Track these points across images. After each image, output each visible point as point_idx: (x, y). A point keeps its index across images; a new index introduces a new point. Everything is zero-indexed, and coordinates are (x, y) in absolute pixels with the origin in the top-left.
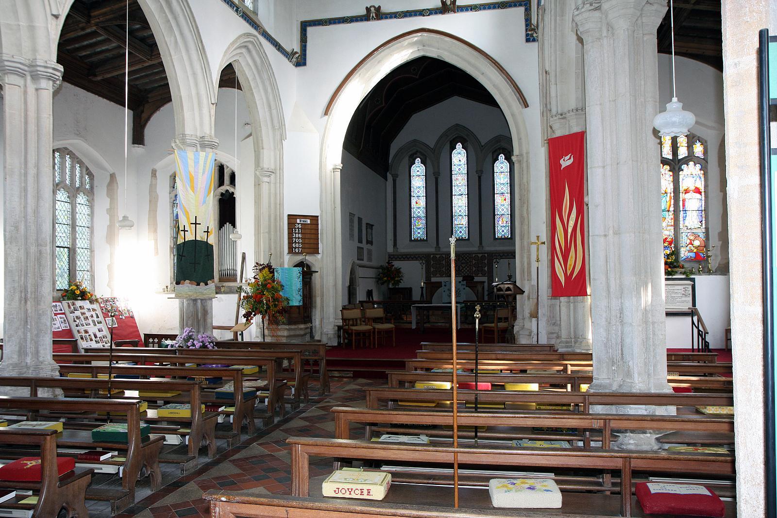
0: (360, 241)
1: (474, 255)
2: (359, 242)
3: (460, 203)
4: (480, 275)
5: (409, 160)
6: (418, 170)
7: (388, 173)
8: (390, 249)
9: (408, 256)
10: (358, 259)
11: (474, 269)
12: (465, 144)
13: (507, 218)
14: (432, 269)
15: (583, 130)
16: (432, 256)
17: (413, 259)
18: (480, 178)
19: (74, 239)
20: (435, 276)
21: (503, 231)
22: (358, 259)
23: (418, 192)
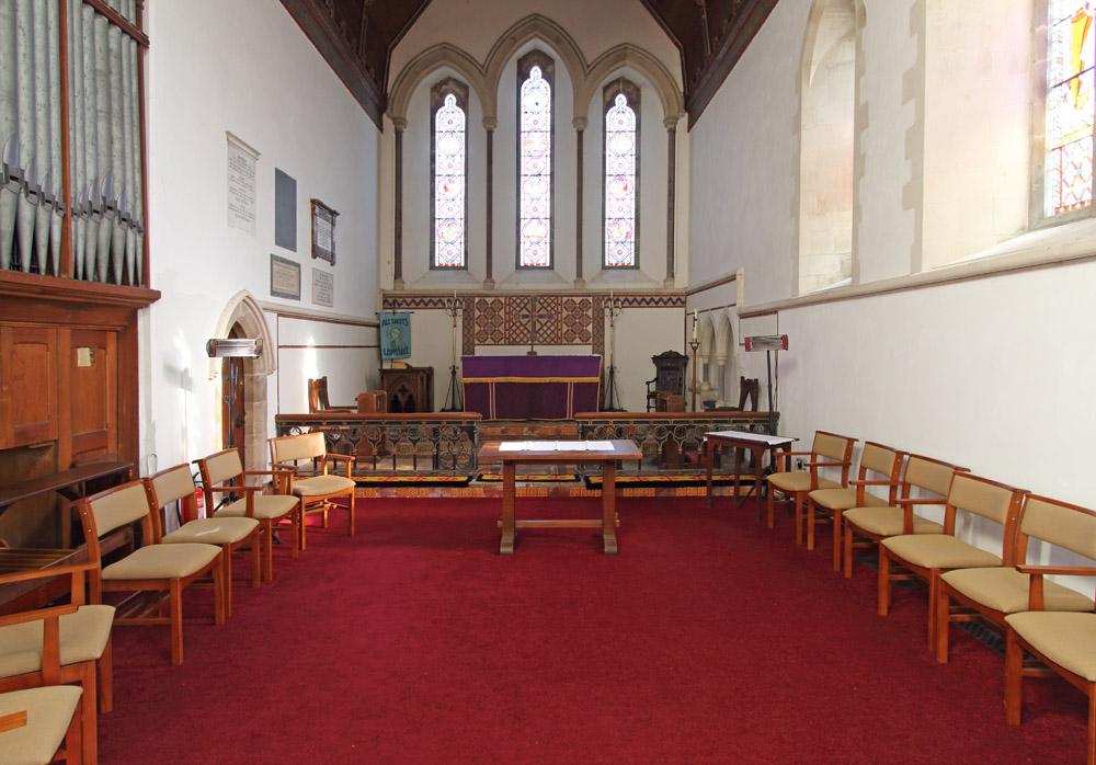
0: (286, 236)
1: (565, 299)
2: (278, 242)
3: (535, 195)
4: (577, 341)
5: (432, 97)
6: (451, 117)
7: (385, 116)
8: (388, 284)
9: (426, 300)
10: (273, 293)
11: (565, 328)
12: (549, 69)
13: (628, 227)
14: (477, 329)
15: (361, 392)
16: (477, 300)
17: (435, 306)
18: (490, 133)
19: (379, 339)
20: (483, 343)
21: (620, 253)
22: (273, 293)
23: (450, 166)
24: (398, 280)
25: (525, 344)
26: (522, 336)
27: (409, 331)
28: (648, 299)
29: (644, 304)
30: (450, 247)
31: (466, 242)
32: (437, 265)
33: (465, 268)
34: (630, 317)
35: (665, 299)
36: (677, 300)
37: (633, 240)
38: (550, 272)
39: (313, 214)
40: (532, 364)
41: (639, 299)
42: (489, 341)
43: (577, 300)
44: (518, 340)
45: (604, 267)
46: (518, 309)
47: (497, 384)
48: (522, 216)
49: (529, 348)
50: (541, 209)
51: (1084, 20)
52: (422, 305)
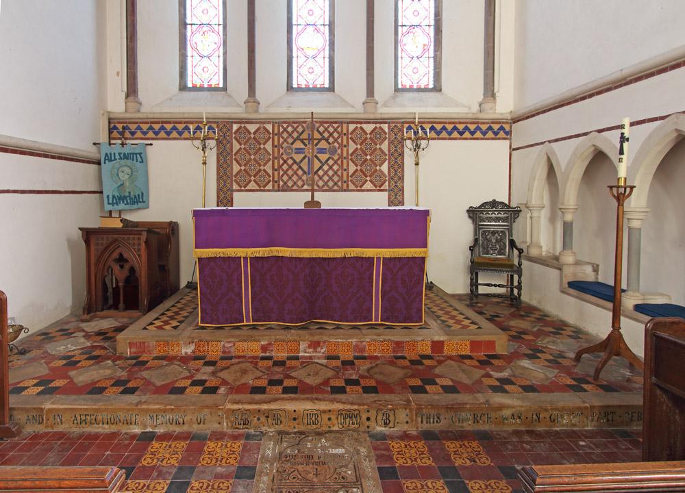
1: (352, 127)
4: (368, 185)
8: (117, 104)
9: (168, 127)
11: (352, 168)
14: (236, 168)
16: (235, 127)
20: (243, 188)
24: (131, 99)
25: (300, 190)
26: (295, 178)
27: (146, 172)
28: (461, 127)
29: (455, 134)
30: (206, 62)
31: (225, 53)
32: (190, 85)
33: (225, 89)
34: (438, 151)
35: (484, 127)
36: (498, 130)
37: (432, 54)
38: (328, 95)
39: (363, 191)
40: (313, 224)
41: (449, 127)
42: (252, 185)
43: (369, 128)
44: (290, 183)
45: (397, 90)
46: (290, 140)
47: (255, 260)
48: (294, 22)
49: (307, 196)
50: (318, 12)
51: (303, 156)
52: (162, 134)
